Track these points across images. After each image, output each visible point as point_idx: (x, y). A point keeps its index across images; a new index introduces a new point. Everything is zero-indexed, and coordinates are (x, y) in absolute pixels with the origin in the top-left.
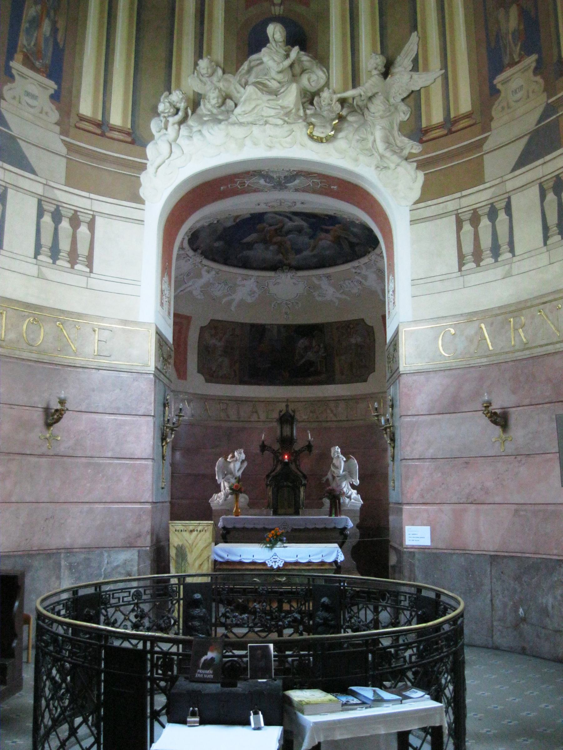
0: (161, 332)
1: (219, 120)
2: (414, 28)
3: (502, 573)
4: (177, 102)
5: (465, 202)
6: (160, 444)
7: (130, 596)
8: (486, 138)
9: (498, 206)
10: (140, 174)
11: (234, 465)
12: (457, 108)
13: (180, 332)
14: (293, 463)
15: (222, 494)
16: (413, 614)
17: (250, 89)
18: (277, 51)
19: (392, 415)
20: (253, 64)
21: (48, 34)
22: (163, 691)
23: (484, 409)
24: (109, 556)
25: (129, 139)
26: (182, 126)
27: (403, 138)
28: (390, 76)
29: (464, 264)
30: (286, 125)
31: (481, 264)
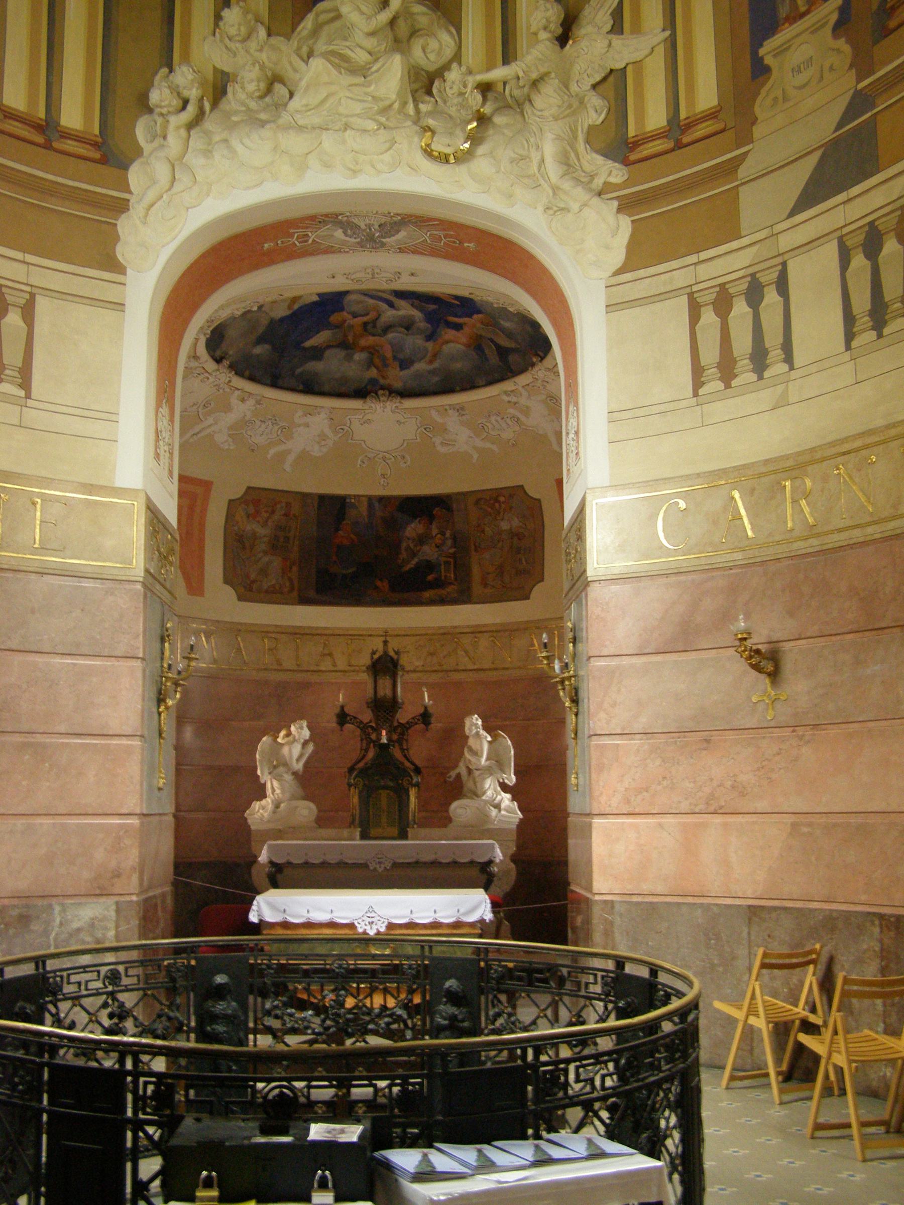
0: (155, 505)
1: (261, 120)
3: (769, 936)
4: (185, 88)
5: (704, 272)
6: (155, 710)
7: (98, 980)
8: (745, 154)
9: (764, 278)
10: (117, 220)
11: (290, 750)
12: (691, 102)
13: (191, 508)
15: (268, 802)
16: (610, 1006)
17: (317, 64)
19: (575, 655)
20: (323, 18)
22: (157, 1147)
23: (737, 643)
24: (64, 910)
25: (97, 155)
27: (595, 155)
28: (571, 42)
29: (703, 383)
30: (382, 131)
31: (734, 383)
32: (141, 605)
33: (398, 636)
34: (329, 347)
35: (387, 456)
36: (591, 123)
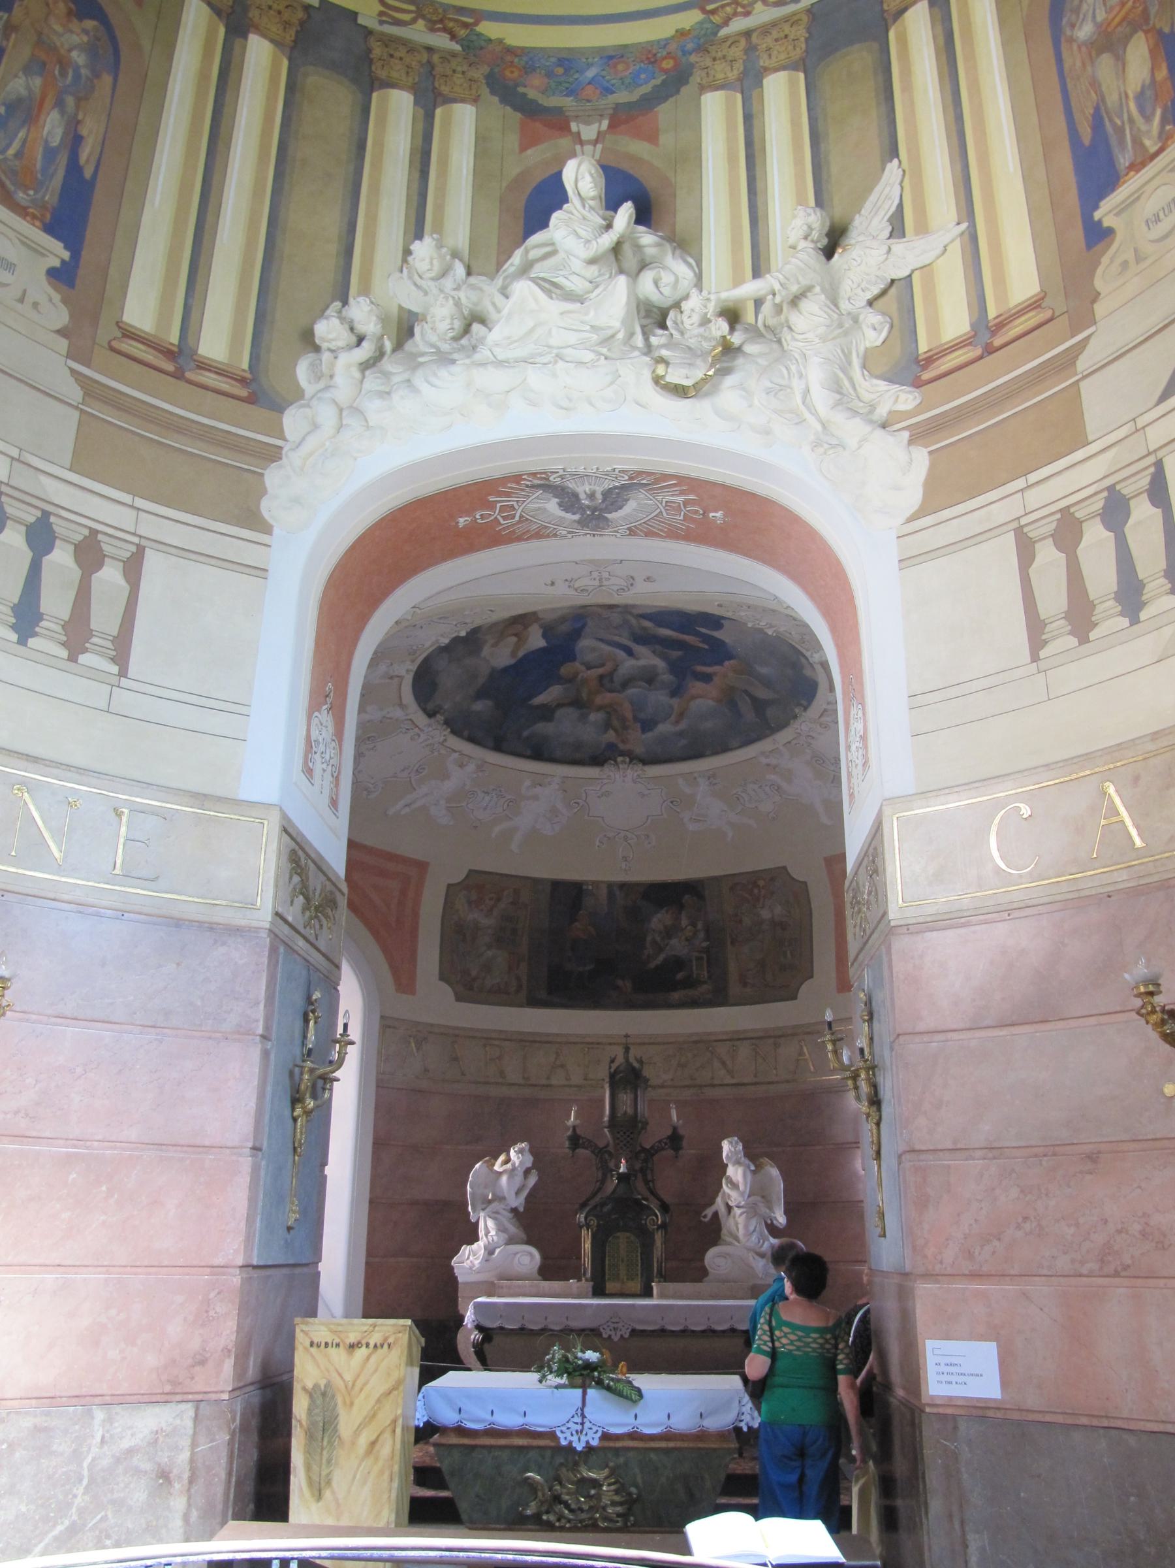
2: (893, 151)
5: (1035, 498)
14: (640, 1175)
15: (479, 1246)
18: (584, 218)
20: (534, 254)
21: (55, 141)
24: (110, 1420)
25: (243, 393)
26: (367, 373)
28: (840, 250)
29: (1046, 642)
32: (265, 960)
33: (644, 1044)
34: (560, 706)
35: (629, 835)
36: (868, 345)
